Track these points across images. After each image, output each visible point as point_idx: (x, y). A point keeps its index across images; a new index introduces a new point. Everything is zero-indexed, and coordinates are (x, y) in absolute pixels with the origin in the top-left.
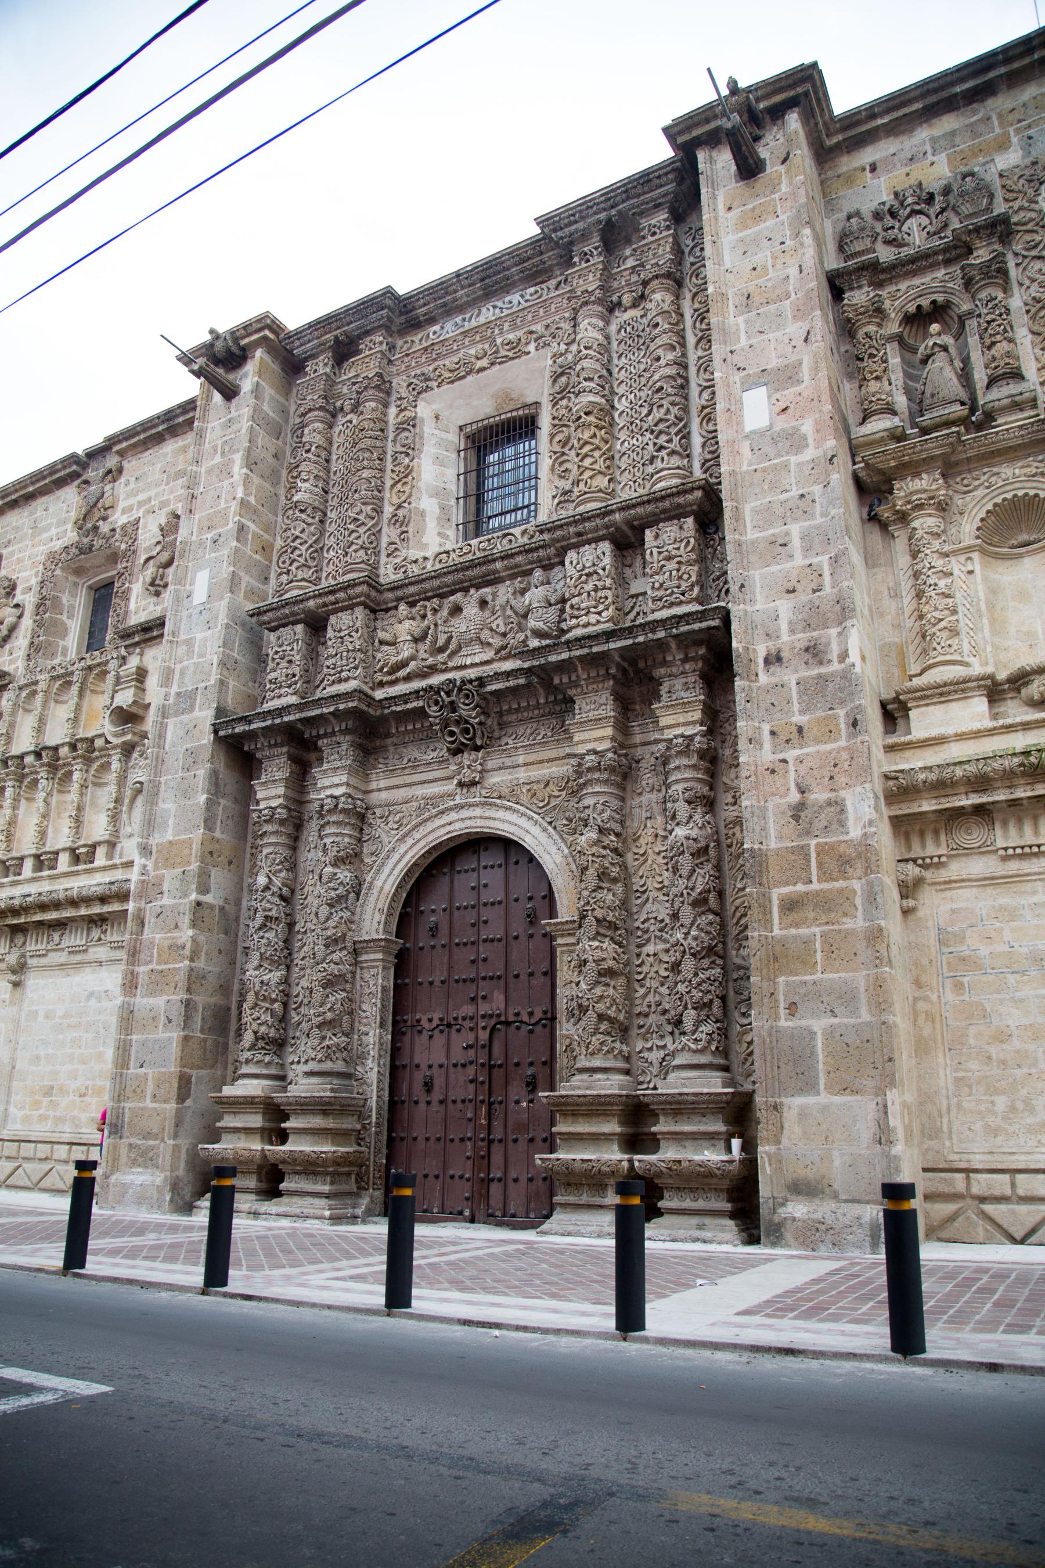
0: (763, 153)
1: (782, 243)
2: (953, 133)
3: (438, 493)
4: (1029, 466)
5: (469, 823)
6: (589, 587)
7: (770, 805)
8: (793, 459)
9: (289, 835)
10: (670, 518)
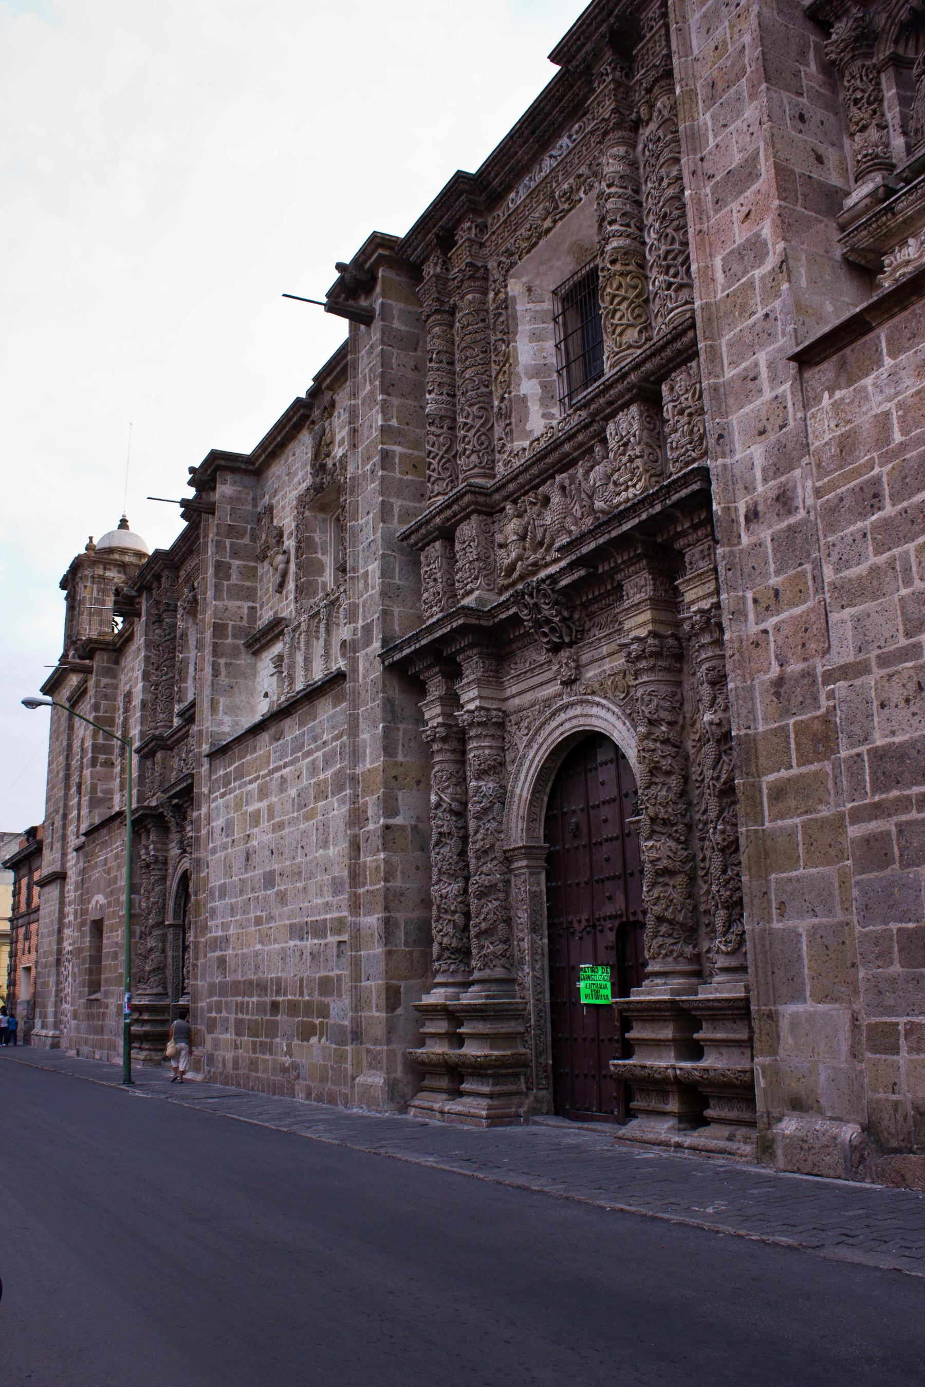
3: (536, 372)
5: (575, 722)
6: (625, 459)
7: (756, 682)
8: (757, 273)
9: (453, 751)
10: (678, 366)
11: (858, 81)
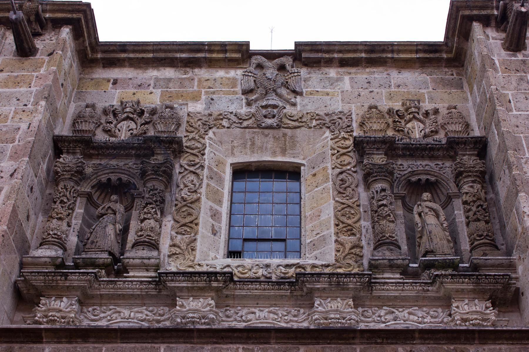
0: (39, 43)
1: (26, 105)
2: (170, 80)
4: (141, 312)
11: (68, 193)
